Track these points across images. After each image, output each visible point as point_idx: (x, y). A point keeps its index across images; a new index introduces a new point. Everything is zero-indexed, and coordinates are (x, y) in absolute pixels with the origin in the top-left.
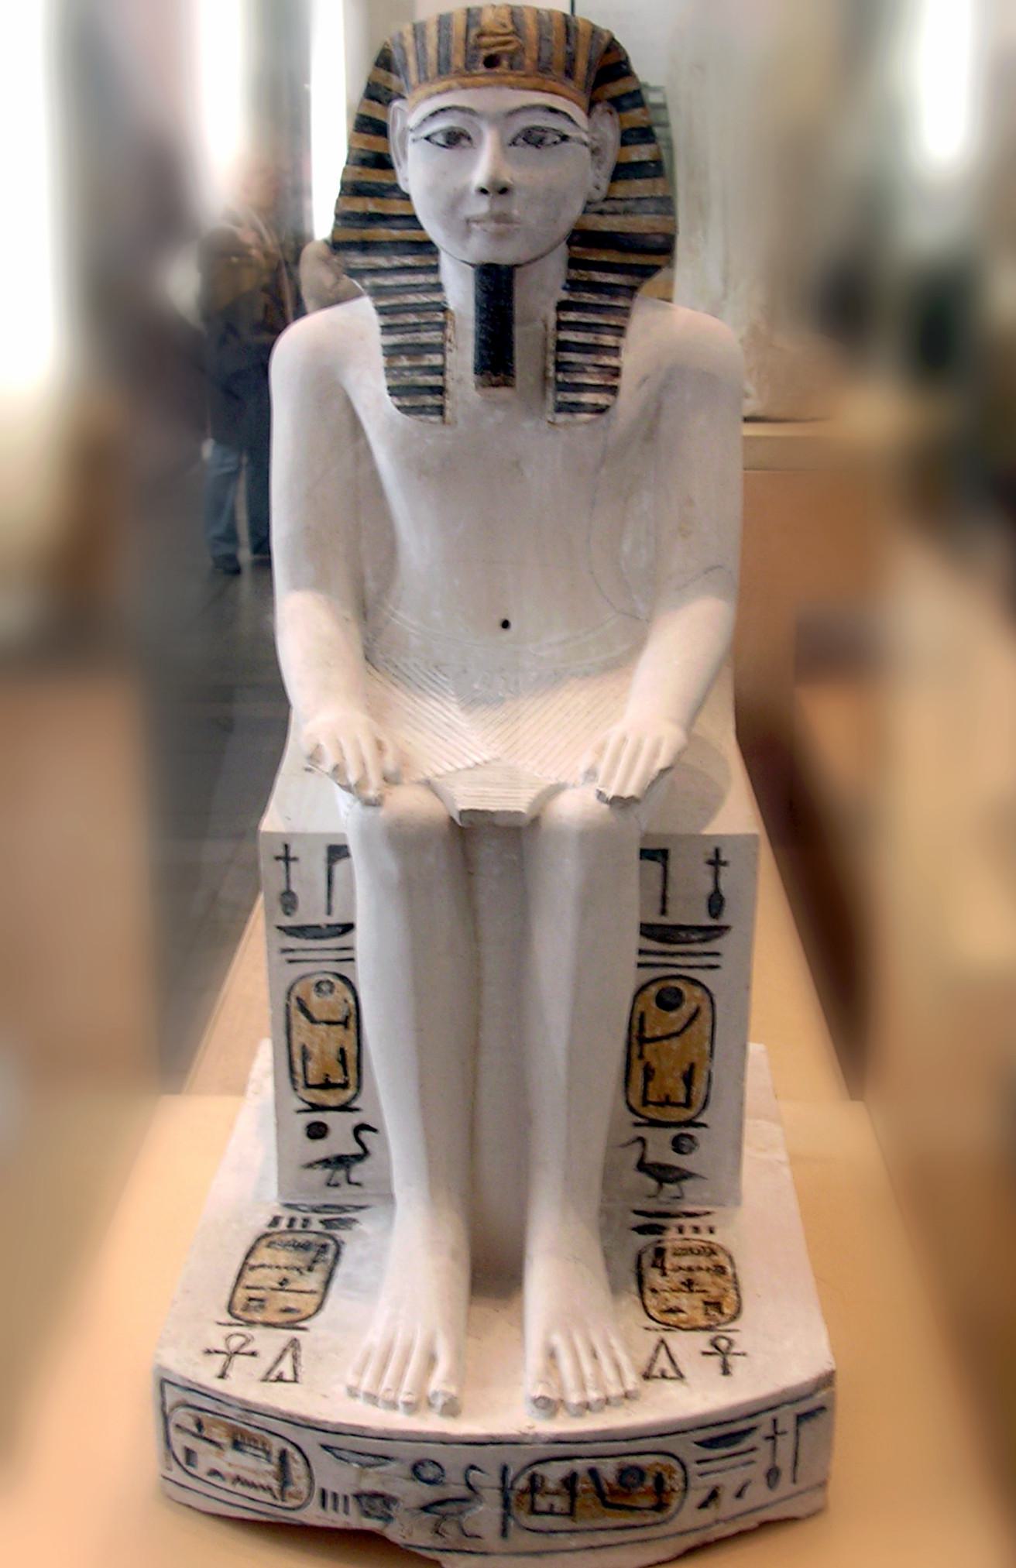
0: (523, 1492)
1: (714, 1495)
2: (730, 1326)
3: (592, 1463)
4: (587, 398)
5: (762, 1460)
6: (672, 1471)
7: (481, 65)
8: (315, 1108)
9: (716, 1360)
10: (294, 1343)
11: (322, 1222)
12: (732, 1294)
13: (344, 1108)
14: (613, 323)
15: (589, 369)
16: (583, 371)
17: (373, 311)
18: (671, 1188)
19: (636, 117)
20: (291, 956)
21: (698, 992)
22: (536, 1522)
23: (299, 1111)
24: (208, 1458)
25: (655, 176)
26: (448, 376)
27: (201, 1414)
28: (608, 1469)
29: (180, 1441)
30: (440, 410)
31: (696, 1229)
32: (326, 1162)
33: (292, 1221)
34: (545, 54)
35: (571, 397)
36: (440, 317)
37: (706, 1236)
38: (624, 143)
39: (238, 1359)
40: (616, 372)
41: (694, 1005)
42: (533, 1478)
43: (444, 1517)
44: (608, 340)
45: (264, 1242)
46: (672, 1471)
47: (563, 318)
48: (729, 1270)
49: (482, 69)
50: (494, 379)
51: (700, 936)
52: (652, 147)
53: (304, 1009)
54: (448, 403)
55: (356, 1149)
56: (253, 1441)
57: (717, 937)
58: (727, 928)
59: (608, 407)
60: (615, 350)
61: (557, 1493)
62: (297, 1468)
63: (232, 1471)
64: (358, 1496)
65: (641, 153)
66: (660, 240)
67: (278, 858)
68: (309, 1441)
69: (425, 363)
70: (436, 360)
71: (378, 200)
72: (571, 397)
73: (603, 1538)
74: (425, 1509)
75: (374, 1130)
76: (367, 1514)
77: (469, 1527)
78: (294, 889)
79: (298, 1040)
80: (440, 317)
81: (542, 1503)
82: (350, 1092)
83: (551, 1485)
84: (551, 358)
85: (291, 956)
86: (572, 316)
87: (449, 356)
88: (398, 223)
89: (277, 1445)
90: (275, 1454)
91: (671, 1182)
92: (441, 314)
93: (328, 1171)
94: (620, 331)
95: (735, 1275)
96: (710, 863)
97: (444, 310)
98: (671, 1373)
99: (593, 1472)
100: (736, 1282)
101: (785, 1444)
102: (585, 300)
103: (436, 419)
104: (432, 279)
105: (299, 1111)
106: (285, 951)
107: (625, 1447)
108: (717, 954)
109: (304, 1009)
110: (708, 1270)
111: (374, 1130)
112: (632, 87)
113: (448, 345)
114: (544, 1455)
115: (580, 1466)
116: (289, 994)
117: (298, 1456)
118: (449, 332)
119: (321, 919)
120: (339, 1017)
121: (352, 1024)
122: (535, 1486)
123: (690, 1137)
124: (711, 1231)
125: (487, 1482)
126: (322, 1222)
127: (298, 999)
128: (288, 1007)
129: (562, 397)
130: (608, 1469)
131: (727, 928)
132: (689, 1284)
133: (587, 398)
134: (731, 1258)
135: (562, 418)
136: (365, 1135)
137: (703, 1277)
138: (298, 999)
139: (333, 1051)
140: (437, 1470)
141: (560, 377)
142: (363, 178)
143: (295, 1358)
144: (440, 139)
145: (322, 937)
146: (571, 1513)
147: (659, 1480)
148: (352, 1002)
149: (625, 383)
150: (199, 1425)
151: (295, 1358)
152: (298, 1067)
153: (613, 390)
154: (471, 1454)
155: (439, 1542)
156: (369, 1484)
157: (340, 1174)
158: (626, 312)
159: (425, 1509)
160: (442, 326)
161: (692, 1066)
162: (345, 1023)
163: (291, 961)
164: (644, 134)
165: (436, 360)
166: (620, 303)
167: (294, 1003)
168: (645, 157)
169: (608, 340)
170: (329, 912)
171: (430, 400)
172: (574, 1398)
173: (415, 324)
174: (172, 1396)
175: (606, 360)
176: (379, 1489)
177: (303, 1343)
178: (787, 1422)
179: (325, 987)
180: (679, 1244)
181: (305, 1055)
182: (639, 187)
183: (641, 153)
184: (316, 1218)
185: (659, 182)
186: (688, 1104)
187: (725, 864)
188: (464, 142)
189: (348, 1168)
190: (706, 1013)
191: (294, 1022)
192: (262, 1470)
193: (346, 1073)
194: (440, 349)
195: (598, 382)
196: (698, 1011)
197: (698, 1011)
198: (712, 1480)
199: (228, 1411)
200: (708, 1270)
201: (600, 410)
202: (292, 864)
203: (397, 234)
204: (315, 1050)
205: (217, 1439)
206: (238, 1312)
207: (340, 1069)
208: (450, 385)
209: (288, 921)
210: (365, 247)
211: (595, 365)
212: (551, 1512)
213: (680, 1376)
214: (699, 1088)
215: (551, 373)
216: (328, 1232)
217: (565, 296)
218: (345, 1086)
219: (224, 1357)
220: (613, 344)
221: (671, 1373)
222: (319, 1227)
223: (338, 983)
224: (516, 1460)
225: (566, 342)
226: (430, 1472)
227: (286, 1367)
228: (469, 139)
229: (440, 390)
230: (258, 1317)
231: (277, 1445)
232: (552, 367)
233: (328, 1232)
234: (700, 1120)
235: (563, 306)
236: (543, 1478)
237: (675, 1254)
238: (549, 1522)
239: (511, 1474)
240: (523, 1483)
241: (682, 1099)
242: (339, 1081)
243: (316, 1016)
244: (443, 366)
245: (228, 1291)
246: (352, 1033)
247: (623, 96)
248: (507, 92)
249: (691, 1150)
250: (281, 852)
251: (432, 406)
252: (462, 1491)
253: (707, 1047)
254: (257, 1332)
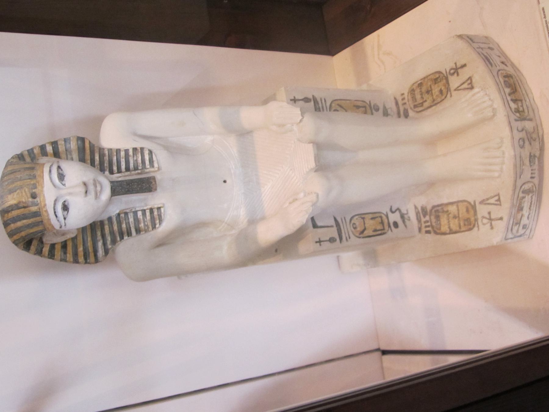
0: (520, 115)
1: (503, 63)
2: (444, 73)
3: (507, 95)
4: (147, 157)
5: (489, 51)
6: (502, 73)
7: (35, 200)
8: (389, 226)
9: (459, 71)
10: (482, 202)
11: (424, 216)
12: (429, 78)
13: (387, 216)
14: (115, 154)
15: (135, 159)
16: (137, 160)
17: (123, 242)
18: (389, 111)
19: (36, 151)
20: (348, 238)
21: (333, 105)
22: (526, 111)
23: (392, 231)
24: (525, 221)
25: (57, 144)
26: (145, 208)
27: (514, 224)
28: (508, 90)
29: (521, 231)
30: (159, 208)
31: (403, 99)
32: (404, 222)
33: (426, 227)
34: (27, 177)
35: (147, 162)
36: (122, 215)
37: (406, 96)
38: (47, 155)
39: (493, 217)
40: (135, 149)
41: (337, 106)
42: (516, 112)
43: (532, 138)
44: (123, 154)
45: (438, 231)
46: (502, 73)
47: (116, 171)
48: (420, 82)
49: (38, 199)
50: (153, 183)
51: (317, 105)
52: (47, 145)
53: (362, 232)
54: (156, 206)
55: (398, 212)
56: (520, 204)
57: (316, 99)
58: (313, 96)
59: (149, 150)
60: (127, 151)
61: (517, 104)
62: (526, 187)
63: (528, 210)
64: (531, 166)
65: (49, 149)
66: (79, 142)
67: (320, 245)
68: (519, 184)
69: (141, 217)
70: (140, 214)
71: (78, 246)
72: (147, 162)
73: (524, 92)
74: (531, 144)
75: (391, 207)
76: (534, 163)
77: (532, 130)
78: (328, 239)
79: (371, 233)
80: (122, 215)
81: (521, 109)
82: (383, 215)
83: (516, 106)
84: (133, 172)
85: (348, 238)
86: (115, 168)
87: (137, 209)
88: (85, 238)
89: (521, 195)
90: (524, 195)
91: (387, 111)
92: (121, 215)
93: (406, 220)
94: (118, 151)
95: (421, 80)
96: (295, 102)
97: (119, 214)
98: (469, 82)
99: (510, 95)
100: (424, 78)
101: (482, 46)
102: (108, 165)
103: (162, 210)
104: (106, 222)
105: (392, 231)
106: (347, 240)
107: (500, 86)
108: (321, 100)
109: (362, 232)
110: (421, 89)
111: (391, 207)
112: (26, 152)
113: (133, 210)
114: (509, 109)
115: (509, 98)
116: (360, 238)
117: (523, 187)
118: (128, 211)
119: (335, 229)
120: (362, 220)
121: (363, 216)
122: (517, 111)
123: (374, 106)
124: (403, 94)
125: (520, 125)
126: (424, 216)
127: (360, 234)
128: (363, 237)
129: (148, 166)
130: (508, 90)
131: (313, 96)
132: (428, 92)
133: (147, 157)
134: (414, 84)
135: (156, 165)
136: (393, 210)
137: (424, 89)
138: (360, 234)
139: (372, 222)
140: (520, 141)
141: (140, 168)
142: (71, 253)
143: (488, 199)
144: (66, 212)
145: (340, 228)
146: (521, 101)
147: (505, 77)
148: (357, 217)
149: (138, 145)
150: (516, 224)
151: (488, 199)
152: (379, 232)
153: (142, 149)
154: (515, 131)
155: (537, 140)
156: (527, 162)
157: (406, 216)
158: (110, 150)
159: (531, 144)
160: (126, 214)
161: (354, 106)
162: (363, 218)
163: (350, 238)
164: (43, 148)
165: (140, 214)
166: (106, 152)
167: (361, 236)
168: (51, 148)
169: (123, 154)
170: (332, 226)
171: (156, 213)
172: (490, 103)
173: (126, 224)
174: (510, 236)
175: (131, 153)
176: (528, 159)
177: (480, 200)
178: (475, 45)
179: (354, 226)
180: (411, 102)
181: (375, 230)
182: (61, 148)
183: (49, 149)
184: (423, 220)
185: (59, 143)
186: (365, 107)
187: (294, 97)
188: (66, 203)
189: (403, 214)
190: (339, 102)
191: (367, 235)
192: (528, 198)
193: (377, 217)
194: (135, 213)
195: (140, 155)
196: (338, 105)
197: (338, 105)
198: (499, 63)
199: (513, 213)
200: (421, 89)
201: (151, 152)
202: (321, 240)
203: (89, 239)
204: (374, 227)
205: (520, 217)
206: (472, 226)
207: (377, 219)
208: (149, 207)
209: (338, 240)
210: (95, 252)
211: (133, 157)
212: (522, 106)
213: (470, 78)
214: (359, 104)
215: (139, 171)
216: (429, 213)
217: (107, 173)
218: (381, 217)
219: (493, 223)
220: (124, 152)
221: (469, 82)
222: (427, 218)
223: (353, 222)
224: (513, 117)
225: (126, 168)
226: (521, 143)
227: (492, 201)
228: (65, 201)
229: (151, 210)
230: (473, 219)
231: (521, 195)
232: (137, 172)
233: (429, 213)
234: (368, 103)
235: (112, 172)
236: (515, 109)
237: (416, 101)
238: (525, 107)
239: (517, 118)
240: (518, 114)
241: (364, 109)
242: (380, 219)
243: (363, 228)
244: (142, 210)
245: (463, 233)
246: (365, 216)
247: (30, 157)
248: (45, 189)
249: (378, 106)
250: (318, 244)
251: (158, 212)
252: (524, 132)
253: (348, 101)
254: (479, 216)
